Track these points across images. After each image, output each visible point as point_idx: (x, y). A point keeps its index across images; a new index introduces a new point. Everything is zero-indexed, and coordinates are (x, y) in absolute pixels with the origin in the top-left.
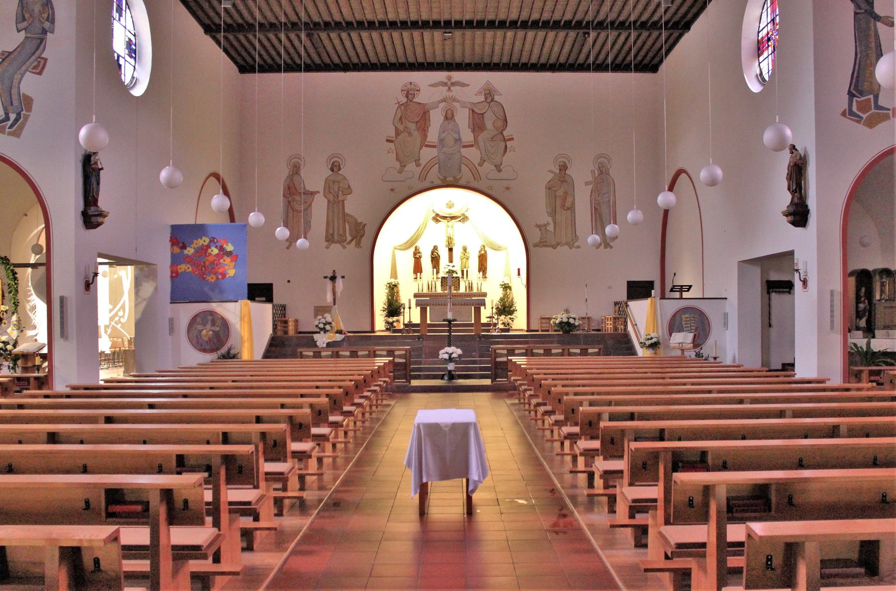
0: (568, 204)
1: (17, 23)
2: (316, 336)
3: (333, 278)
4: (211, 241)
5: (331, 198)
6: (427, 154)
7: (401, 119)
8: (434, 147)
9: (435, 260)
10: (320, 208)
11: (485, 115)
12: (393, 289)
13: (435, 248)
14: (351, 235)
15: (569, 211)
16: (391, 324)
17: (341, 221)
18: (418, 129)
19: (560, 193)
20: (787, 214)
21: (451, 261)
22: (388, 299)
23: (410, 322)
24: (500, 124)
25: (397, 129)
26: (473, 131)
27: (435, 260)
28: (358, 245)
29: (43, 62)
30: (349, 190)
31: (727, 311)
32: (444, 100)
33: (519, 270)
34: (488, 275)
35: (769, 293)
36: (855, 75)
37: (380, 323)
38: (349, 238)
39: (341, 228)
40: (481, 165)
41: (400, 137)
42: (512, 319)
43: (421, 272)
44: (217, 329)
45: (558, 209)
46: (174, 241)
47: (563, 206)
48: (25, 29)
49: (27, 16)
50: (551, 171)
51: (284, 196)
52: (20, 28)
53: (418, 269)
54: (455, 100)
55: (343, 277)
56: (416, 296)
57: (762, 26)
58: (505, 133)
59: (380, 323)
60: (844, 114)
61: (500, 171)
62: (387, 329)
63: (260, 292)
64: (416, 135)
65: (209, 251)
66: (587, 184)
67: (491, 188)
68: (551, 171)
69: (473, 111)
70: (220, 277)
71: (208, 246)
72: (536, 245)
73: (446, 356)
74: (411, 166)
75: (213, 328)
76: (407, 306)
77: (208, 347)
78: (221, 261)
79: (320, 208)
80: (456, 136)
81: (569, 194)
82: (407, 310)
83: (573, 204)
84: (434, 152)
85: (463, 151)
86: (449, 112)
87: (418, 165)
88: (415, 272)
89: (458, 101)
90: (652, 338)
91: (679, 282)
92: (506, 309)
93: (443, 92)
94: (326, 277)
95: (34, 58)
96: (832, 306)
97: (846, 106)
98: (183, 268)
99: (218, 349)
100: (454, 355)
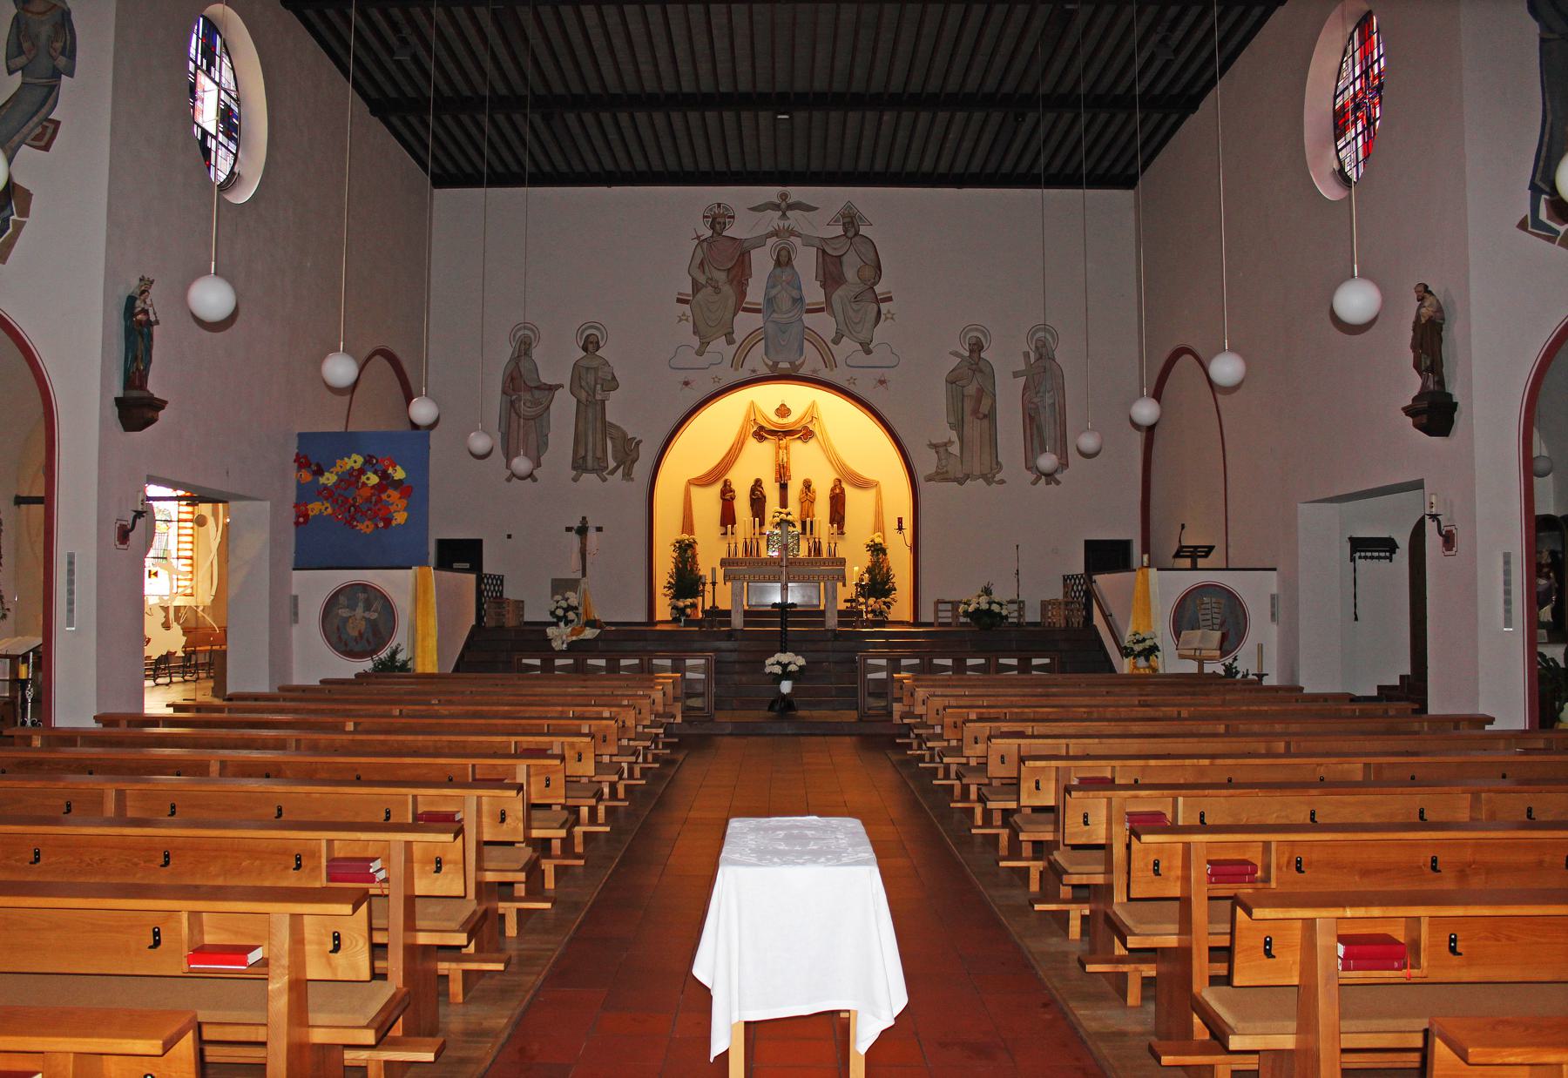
0: (984, 409)
1: (7, 58)
2: (551, 631)
3: (582, 531)
4: (366, 462)
5: (583, 395)
6: (745, 324)
7: (702, 264)
8: (758, 311)
9: (757, 501)
10: (564, 407)
11: (845, 259)
12: (685, 551)
13: (758, 483)
14: (615, 458)
15: (986, 422)
16: (682, 611)
17: (599, 436)
18: (731, 282)
19: (971, 389)
20: (1408, 411)
21: (784, 504)
22: (677, 567)
23: (714, 607)
24: (869, 273)
25: (695, 283)
26: (824, 286)
27: (757, 501)
28: (628, 475)
29: (52, 127)
30: (613, 384)
31: (294, 592)
32: (775, 233)
33: (900, 520)
34: (846, 529)
35: (1353, 559)
36: (1543, 153)
37: (663, 611)
38: (612, 464)
39: (599, 447)
40: (836, 341)
41: (699, 296)
42: (888, 605)
43: (733, 523)
44: (374, 616)
45: (968, 418)
46: (302, 462)
47: (975, 412)
48: (22, 69)
49: (26, 45)
50: (956, 354)
51: (504, 392)
52: (13, 67)
53: (728, 517)
54: (792, 233)
55: (599, 529)
56: (723, 563)
57: (1341, 86)
58: (878, 289)
59: (663, 611)
60: (1522, 225)
61: (868, 352)
62: (676, 620)
63: (460, 554)
64: (727, 290)
65: (364, 478)
66: (1016, 375)
67: (852, 380)
68: (956, 354)
69: (824, 251)
70: (381, 524)
71: (362, 471)
72: (929, 479)
73: (778, 670)
74: (719, 344)
75: (367, 615)
76: (709, 580)
77: (358, 648)
78: (384, 496)
79: (564, 407)
80: (795, 293)
81: (986, 392)
82: (709, 587)
83: (993, 408)
84: (757, 320)
85: (806, 317)
86: (784, 253)
87: (730, 342)
88: (724, 523)
89: (799, 235)
90: (1144, 640)
91: (1190, 540)
92: (878, 584)
93: (772, 219)
94: (569, 529)
95: (35, 119)
96: (1507, 583)
97: (1527, 211)
98: (315, 508)
99: (375, 651)
100: (792, 668)
